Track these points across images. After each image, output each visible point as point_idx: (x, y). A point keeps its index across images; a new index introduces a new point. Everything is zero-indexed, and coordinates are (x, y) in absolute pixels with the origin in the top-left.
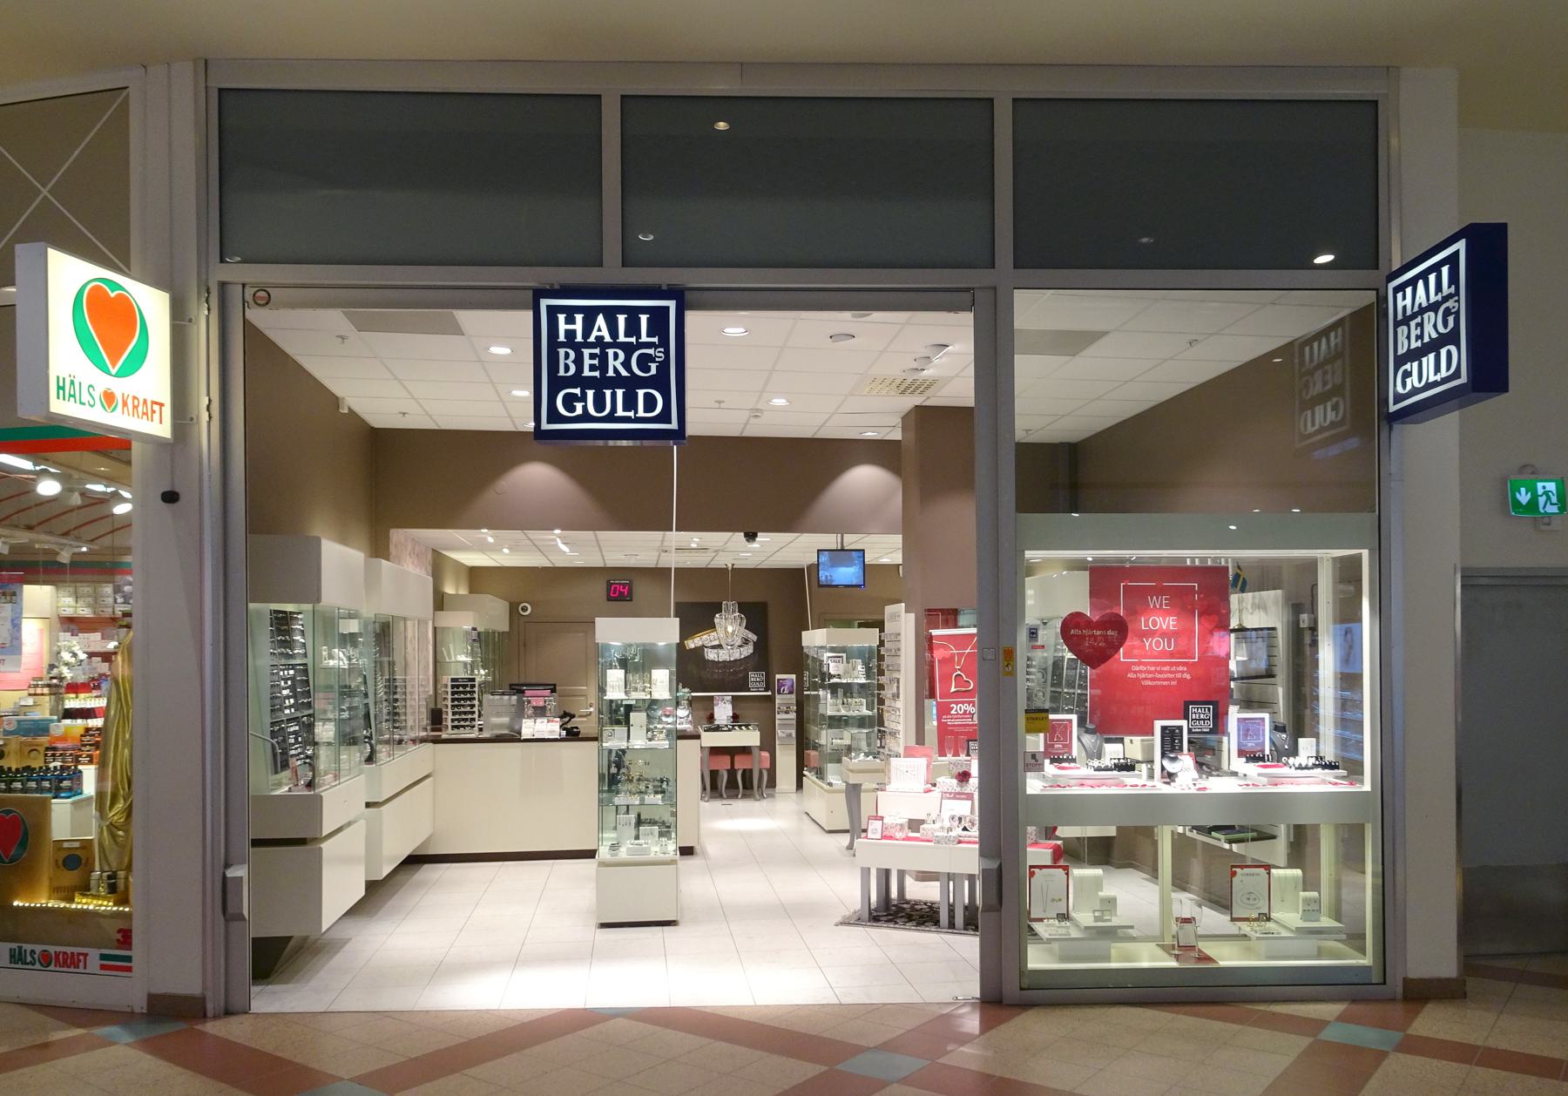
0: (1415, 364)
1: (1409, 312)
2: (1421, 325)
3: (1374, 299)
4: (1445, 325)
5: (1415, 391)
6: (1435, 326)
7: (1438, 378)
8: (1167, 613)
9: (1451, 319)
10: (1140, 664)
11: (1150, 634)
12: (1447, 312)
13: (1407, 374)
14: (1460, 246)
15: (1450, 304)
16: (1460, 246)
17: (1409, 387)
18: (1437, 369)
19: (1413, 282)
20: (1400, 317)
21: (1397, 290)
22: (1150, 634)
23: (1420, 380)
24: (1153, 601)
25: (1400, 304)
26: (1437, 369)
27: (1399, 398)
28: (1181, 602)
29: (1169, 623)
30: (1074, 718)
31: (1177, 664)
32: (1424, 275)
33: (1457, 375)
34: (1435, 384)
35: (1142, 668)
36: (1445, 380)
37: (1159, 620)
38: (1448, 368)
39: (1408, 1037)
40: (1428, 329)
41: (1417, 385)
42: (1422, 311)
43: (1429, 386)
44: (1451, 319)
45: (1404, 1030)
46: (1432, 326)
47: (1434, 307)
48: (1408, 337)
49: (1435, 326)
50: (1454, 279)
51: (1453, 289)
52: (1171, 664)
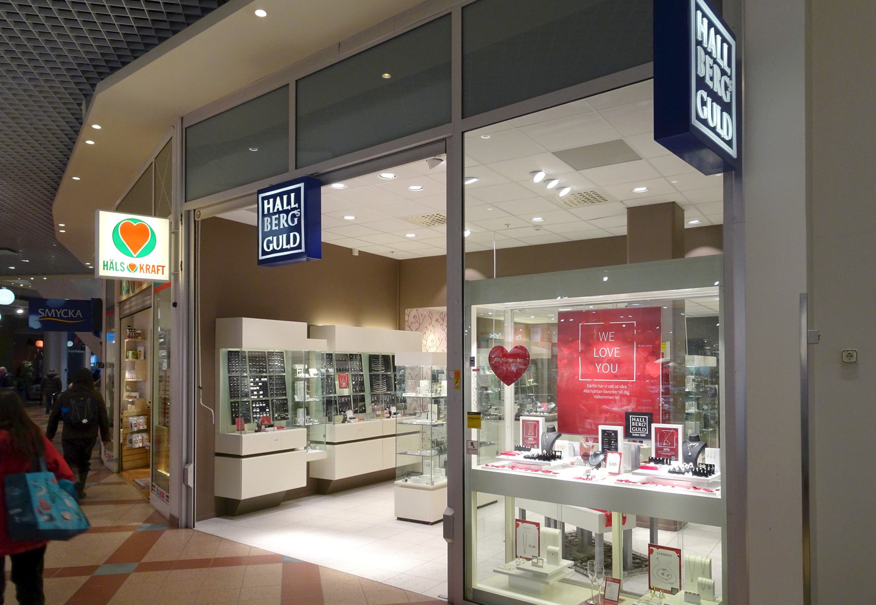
0: (275, 238)
1: (271, 211)
2: (279, 219)
3: (334, 193)
4: (293, 222)
5: (274, 251)
6: (287, 221)
7: (288, 247)
8: (612, 345)
9: (296, 220)
10: (592, 383)
11: (600, 361)
12: (294, 216)
13: (269, 242)
14: (302, 185)
15: (295, 212)
16: (302, 185)
17: (271, 248)
18: (288, 243)
19: (274, 197)
20: (266, 212)
21: (264, 199)
22: (600, 361)
23: (278, 246)
24: (603, 336)
25: (266, 206)
26: (288, 243)
27: (264, 253)
28: (623, 337)
29: (613, 351)
30: (620, 430)
31: (620, 384)
32: (281, 195)
33: (299, 247)
34: (287, 250)
35: (594, 386)
36: (292, 249)
37: (607, 350)
38: (294, 243)
39: (139, 561)
40: (283, 221)
41: (276, 248)
42: (279, 212)
43: (282, 250)
44: (296, 220)
45: (139, 561)
46: (284, 221)
47: (287, 212)
48: (271, 223)
49: (287, 221)
50: (298, 200)
51: (297, 205)
52: (616, 383)
